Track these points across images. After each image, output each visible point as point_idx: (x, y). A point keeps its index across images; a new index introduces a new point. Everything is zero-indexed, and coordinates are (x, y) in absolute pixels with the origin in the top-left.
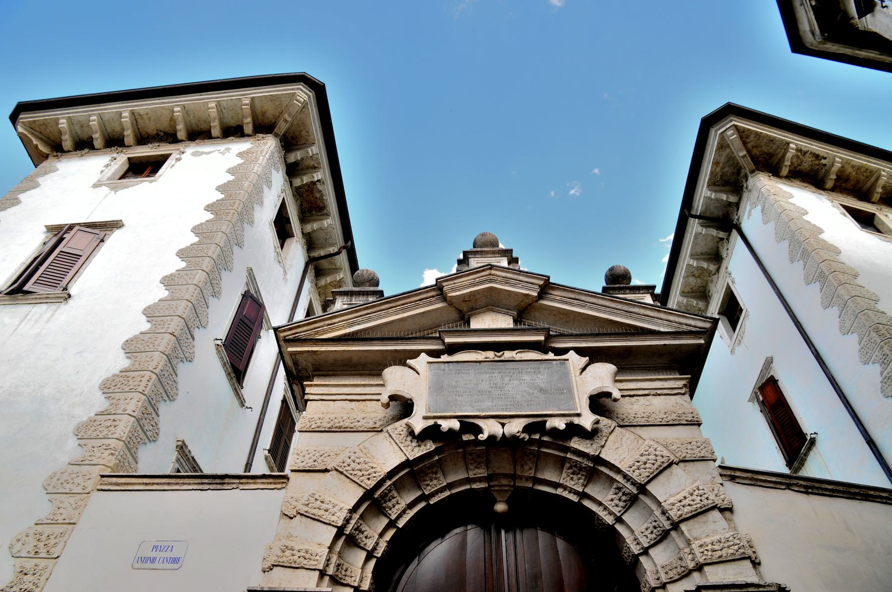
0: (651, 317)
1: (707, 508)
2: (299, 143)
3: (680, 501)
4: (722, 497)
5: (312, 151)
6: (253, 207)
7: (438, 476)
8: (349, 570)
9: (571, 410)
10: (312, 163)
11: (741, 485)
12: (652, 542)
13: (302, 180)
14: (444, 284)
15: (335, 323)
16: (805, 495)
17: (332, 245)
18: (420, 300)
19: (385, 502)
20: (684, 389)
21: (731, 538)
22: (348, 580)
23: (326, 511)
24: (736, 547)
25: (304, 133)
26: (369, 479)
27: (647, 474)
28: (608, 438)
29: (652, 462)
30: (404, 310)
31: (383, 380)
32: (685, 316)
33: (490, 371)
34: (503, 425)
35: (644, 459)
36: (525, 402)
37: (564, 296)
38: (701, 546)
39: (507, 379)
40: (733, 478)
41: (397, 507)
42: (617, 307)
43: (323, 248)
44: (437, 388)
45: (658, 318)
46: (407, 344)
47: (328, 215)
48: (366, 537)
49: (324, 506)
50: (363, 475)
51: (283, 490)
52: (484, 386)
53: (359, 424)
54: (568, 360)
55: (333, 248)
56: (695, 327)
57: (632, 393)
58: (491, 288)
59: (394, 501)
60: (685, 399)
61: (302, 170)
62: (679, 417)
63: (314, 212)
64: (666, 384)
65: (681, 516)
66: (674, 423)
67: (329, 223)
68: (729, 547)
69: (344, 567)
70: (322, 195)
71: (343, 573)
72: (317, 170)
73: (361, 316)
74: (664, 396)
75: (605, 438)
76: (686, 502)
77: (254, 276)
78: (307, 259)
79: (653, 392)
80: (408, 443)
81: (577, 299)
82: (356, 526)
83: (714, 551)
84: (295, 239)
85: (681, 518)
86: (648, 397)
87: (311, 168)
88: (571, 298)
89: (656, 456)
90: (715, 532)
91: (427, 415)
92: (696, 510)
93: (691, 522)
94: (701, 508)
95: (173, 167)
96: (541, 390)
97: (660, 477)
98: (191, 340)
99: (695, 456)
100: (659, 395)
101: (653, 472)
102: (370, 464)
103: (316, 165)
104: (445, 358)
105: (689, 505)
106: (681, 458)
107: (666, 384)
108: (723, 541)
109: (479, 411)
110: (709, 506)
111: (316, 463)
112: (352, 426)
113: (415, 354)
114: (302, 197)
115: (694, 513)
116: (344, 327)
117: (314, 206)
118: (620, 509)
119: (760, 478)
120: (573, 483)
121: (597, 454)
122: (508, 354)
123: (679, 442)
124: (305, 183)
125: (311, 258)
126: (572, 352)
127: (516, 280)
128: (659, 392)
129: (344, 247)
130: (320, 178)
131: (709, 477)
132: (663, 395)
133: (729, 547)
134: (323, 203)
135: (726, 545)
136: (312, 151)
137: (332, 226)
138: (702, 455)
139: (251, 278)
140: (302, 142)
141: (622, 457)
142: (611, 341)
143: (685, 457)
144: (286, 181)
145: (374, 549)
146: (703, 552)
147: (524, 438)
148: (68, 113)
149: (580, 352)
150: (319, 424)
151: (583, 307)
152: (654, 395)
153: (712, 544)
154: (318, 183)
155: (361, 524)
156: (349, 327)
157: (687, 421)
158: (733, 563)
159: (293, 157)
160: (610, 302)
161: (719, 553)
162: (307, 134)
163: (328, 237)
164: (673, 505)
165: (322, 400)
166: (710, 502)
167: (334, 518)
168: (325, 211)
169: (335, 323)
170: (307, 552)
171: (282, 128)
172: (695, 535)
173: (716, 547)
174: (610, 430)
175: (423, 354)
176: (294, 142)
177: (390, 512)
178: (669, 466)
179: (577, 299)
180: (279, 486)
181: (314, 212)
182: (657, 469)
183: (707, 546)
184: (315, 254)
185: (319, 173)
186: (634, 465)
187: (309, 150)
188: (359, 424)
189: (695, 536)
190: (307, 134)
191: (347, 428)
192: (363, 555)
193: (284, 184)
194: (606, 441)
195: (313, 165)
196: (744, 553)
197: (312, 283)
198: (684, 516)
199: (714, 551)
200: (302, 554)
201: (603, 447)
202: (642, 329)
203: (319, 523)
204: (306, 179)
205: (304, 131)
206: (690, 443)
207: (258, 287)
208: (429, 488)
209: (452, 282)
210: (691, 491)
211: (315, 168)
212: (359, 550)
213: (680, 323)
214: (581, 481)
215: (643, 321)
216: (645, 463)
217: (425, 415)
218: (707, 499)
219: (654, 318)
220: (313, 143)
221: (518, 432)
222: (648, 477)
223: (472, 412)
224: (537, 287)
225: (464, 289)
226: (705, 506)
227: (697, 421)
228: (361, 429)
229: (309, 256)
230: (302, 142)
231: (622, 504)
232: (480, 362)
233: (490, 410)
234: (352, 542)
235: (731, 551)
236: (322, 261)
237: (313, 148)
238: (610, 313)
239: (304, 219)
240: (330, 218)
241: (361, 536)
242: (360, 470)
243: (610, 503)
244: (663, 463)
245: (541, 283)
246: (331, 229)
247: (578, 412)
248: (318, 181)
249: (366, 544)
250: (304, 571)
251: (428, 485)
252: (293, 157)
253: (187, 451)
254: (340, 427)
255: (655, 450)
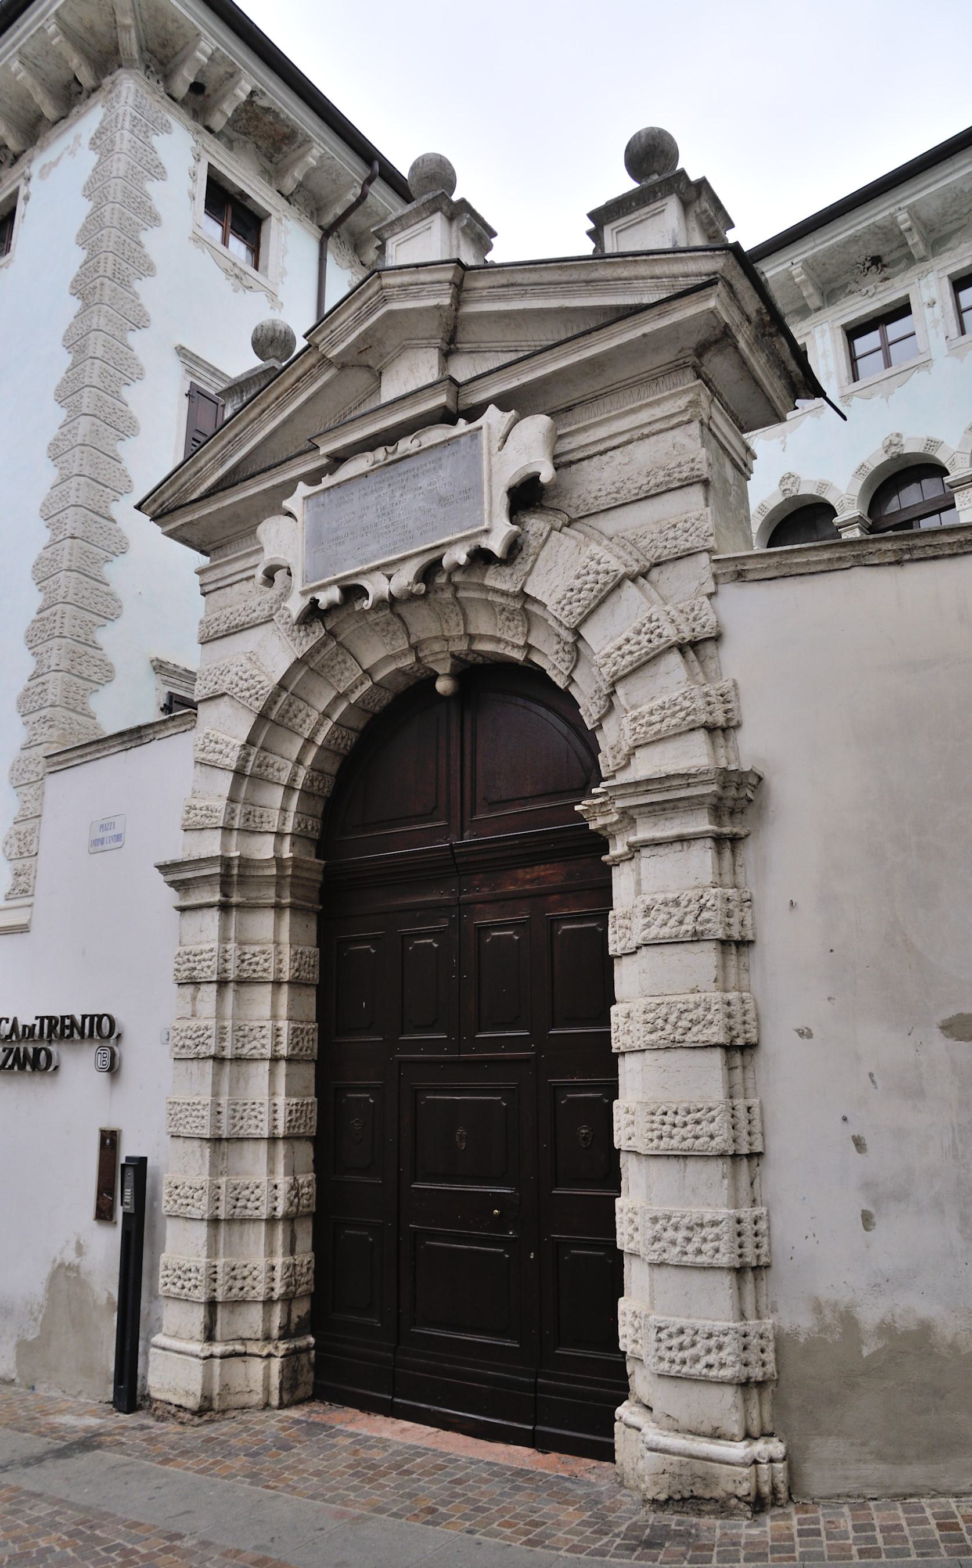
0: (625, 279)
1: (657, 651)
2: (178, 48)
3: (619, 648)
4: (703, 620)
5: (203, 53)
6: (139, 244)
7: (349, 663)
8: (265, 815)
9: (477, 526)
10: (221, 70)
11: (756, 584)
12: (603, 711)
13: (223, 113)
14: (318, 340)
15: (202, 468)
16: (893, 569)
17: (350, 186)
18: (298, 380)
19: (290, 720)
20: (691, 410)
21: (680, 699)
22: (266, 827)
23: (221, 752)
24: (683, 714)
25: (171, 26)
26: (257, 699)
27: (579, 610)
28: (538, 555)
29: (588, 586)
30: (281, 407)
31: (259, 543)
32: (677, 258)
33: (378, 486)
34: (390, 578)
35: (578, 584)
36: (418, 528)
37: (492, 284)
38: (635, 719)
39: (398, 494)
40: (740, 576)
41: (308, 721)
42: (571, 279)
43: (338, 199)
44: (316, 541)
45: (637, 278)
46: (284, 472)
47: (308, 141)
48: (279, 770)
49: (218, 747)
50: (251, 696)
51: (194, 731)
52: (370, 517)
53: (255, 615)
54: (481, 428)
55: (352, 191)
56: (700, 274)
57: (601, 447)
58: (390, 314)
59: (301, 716)
60: (690, 432)
61: (216, 91)
62: (669, 475)
63: (285, 148)
64: (658, 412)
65: (615, 673)
66: (659, 490)
67: (318, 154)
68: (673, 715)
69: (257, 814)
70: (276, 115)
71: (257, 820)
72: (236, 78)
73: (229, 442)
74: (655, 438)
75: (532, 558)
76: (626, 648)
77: (193, 354)
78: (319, 234)
79: (637, 434)
80: (295, 634)
81: (512, 285)
82: (257, 762)
83: (651, 724)
84: (273, 220)
85: (615, 678)
86: (630, 446)
87: (227, 79)
88: (503, 286)
89: (598, 573)
90: (664, 690)
91: (305, 588)
92: (639, 659)
93: (632, 681)
94: (647, 653)
95: (26, 218)
96: (443, 501)
97: (604, 610)
98: (111, 524)
99: (676, 550)
100: (648, 436)
101: (589, 604)
102: (257, 679)
103: (230, 70)
104: (327, 481)
105: (631, 653)
106: (653, 560)
107: (658, 412)
108: (667, 706)
109: (362, 564)
110: (661, 648)
111: (217, 686)
112: (248, 619)
113: (288, 488)
114: (249, 133)
115: (635, 665)
116: (215, 469)
117: (276, 138)
118: (567, 664)
119: (796, 561)
120: (511, 633)
121: (517, 589)
122: (406, 445)
123: (655, 529)
124: (230, 115)
125: (326, 227)
126: (492, 407)
127: (417, 284)
128: (646, 431)
129: (369, 181)
130: (249, 89)
131: (696, 584)
132: (654, 434)
133: (673, 715)
134: (288, 126)
135: (669, 712)
136: (203, 53)
137: (327, 156)
138: (688, 545)
139: (191, 360)
140: (181, 43)
141: (554, 585)
142: (556, 359)
143: (659, 557)
144: (198, 133)
145: (293, 778)
146: (635, 729)
147: (419, 590)
148: (26, 32)
149: (503, 402)
150: (216, 628)
151: (523, 295)
152: (639, 439)
153: (651, 713)
154: (255, 98)
155: (265, 758)
156: (222, 465)
157: (679, 480)
158: (678, 738)
159: (185, 77)
160: (560, 272)
161: (657, 727)
162: (176, 25)
163: (334, 176)
164: (608, 656)
165: (219, 588)
166: (663, 640)
167: (227, 761)
168: (300, 138)
169: (202, 468)
170: (207, 809)
171: (130, 43)
172: (633, 700)
173: (654, 718)
174: (541, 541)
175: (301, 485)
176: (169, 51)
177: (300, 730)
178: (618, 585)
179: (512, 285)
180: (188, 726)
181: (285, 148)
182: (596, 597)
183: (644, 717)
184: (329, 219)
185: (243, 82)
186: (564, 597)
187: (198, 54)
188: (255, 615)
189: (634, 703)
190: (176, 25)
191: (243, 624)
192: (280, 792)
193: (197, 141)
194: (536, 560)
195: (226, 72)
196: (693, 720)
197: (352, 267)
198: (621, 673)
199: (651, 724)
200: (204, 812)
201: (529, 573)
202: (617, 308)
203: (217, 770)
204: (228, 108)
205: (169, 23)
206: (675, 526)
207: (211, 366)
208: (342, 684)
209: (328, 331)
210: (639, 627)
211: (232, 75)
212: (275, 786)
213: (675, 276)
214: (520, 629)
215: (615, 292)
216: (580, 591)
217: (302, 589)
218: (660, 636)
219: (630, 279)
220: (198, 35)
221: (409, 584)
222: (580, 614)
223: (354, 567)
224: (446, 286)
225: (348, 334)
226: (653, 649)
227: (697, 476)
228: (258, 622)
229: (320, 227)
230: (181, 43)
231: (567, 657)
232: (365, 475)
233: (375, 557)
234: (259, 779)
235: (674, 721)
236: (353, 217)
237: (202, 44)
238: (565, 294)
239: (273, 171)
240: (315, 145)
241: (270, 770)
242: (248, 689)
243: (555, 657)
244: (605, 584)
245: (449, 275)
246: (329, 161)
247: (485, 527)
248: (252, 93)
249: (279, 779)
250: (209, 831)
251: (340, 680)
252: (185, 77)
253: (170, 667)
254: (237, 626)
255: (599, 563)
